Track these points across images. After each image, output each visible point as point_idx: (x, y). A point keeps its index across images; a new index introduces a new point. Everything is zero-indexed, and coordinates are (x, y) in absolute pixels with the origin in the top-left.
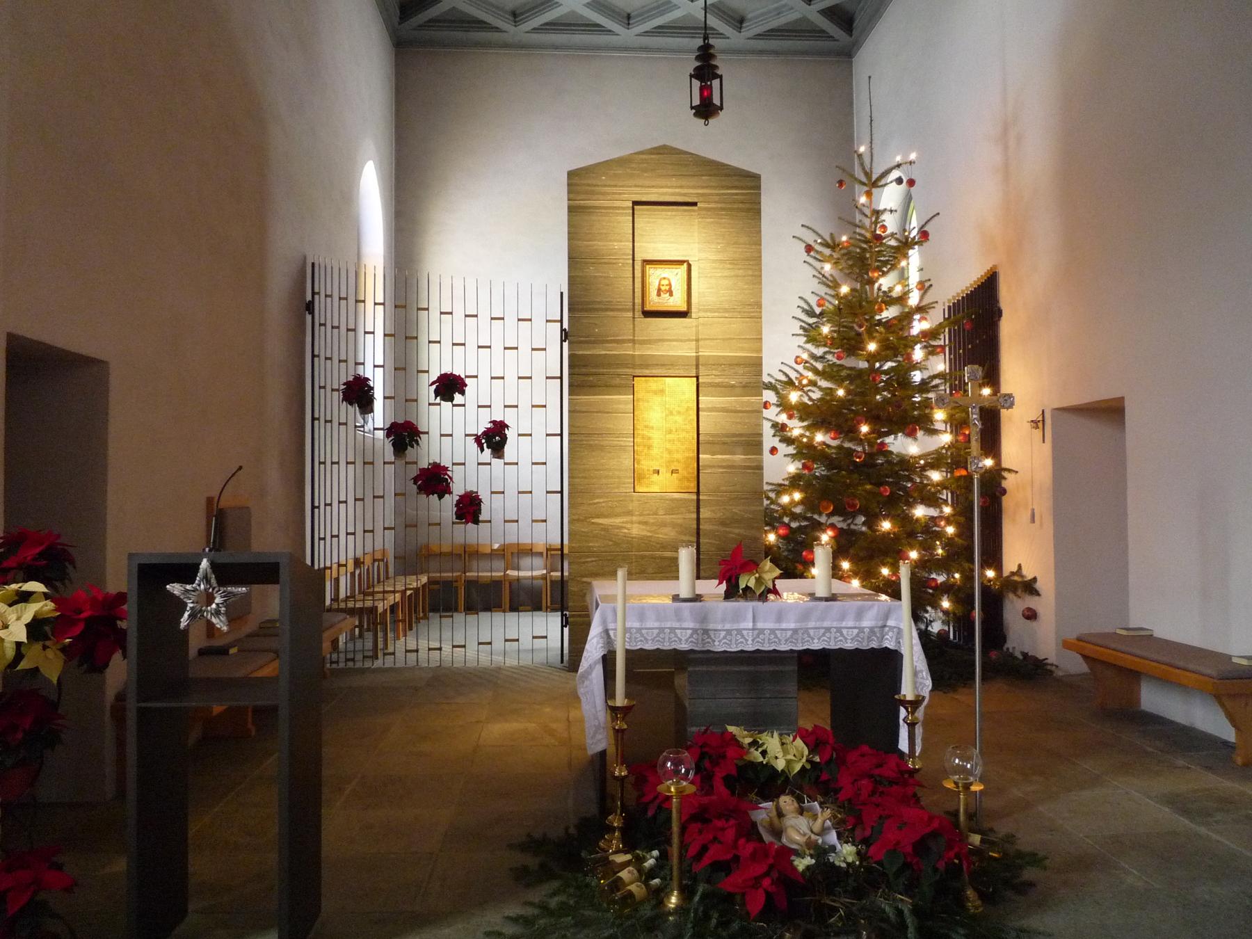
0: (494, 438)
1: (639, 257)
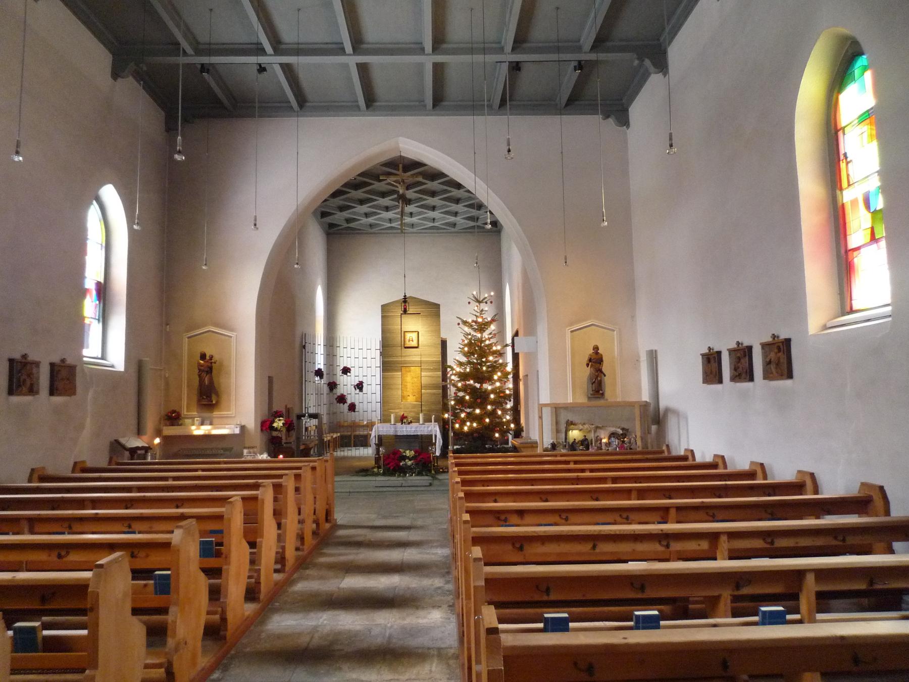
0: (360, 386)
1: (403, 330)
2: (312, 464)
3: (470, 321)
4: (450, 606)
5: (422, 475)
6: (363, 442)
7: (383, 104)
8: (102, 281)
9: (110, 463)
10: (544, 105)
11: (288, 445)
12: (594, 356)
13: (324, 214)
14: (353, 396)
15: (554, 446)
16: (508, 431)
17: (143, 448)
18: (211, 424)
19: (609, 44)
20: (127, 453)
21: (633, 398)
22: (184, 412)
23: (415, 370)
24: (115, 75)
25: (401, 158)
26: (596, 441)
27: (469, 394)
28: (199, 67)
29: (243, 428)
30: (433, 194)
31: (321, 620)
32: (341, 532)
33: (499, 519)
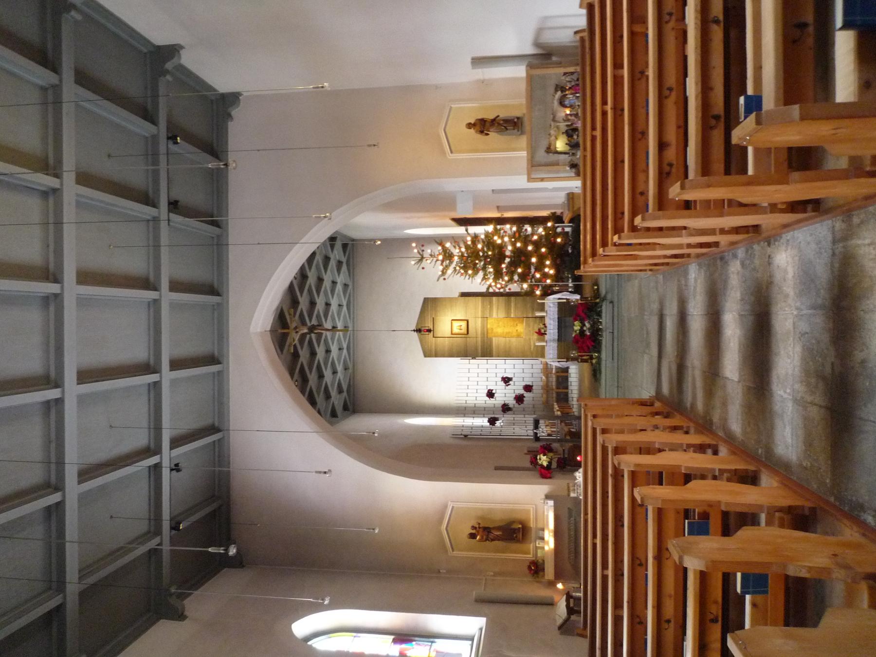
0: (506, 380)
2: (590, 417)
3: (441, 268)
4: (769, 245)
5: (601, 312)
6: (563, 376)
7: (216, 346)
8: (392, 637)
9: (583, 636)
10: (217, 182)
11: (566, 452)
12: (478, 127)
13: (334, 414)
14: (517, 387)
15: (573, 166)
16: (554, 228)
17: (568, 601)
18: (543, 530)
19: (149, 107)
20: (573, 617)
21: (523, 86)
22: (530, 557)
23: (491, 324)
24: (180, 616)
25: (273, 331)
26: (568, 120)
27: (516, 269)
28: (174, 532)
29: (548, 497)
30: (313, 304)
31: (785, 396)
32: (665, 390)
33: (668, 174)
